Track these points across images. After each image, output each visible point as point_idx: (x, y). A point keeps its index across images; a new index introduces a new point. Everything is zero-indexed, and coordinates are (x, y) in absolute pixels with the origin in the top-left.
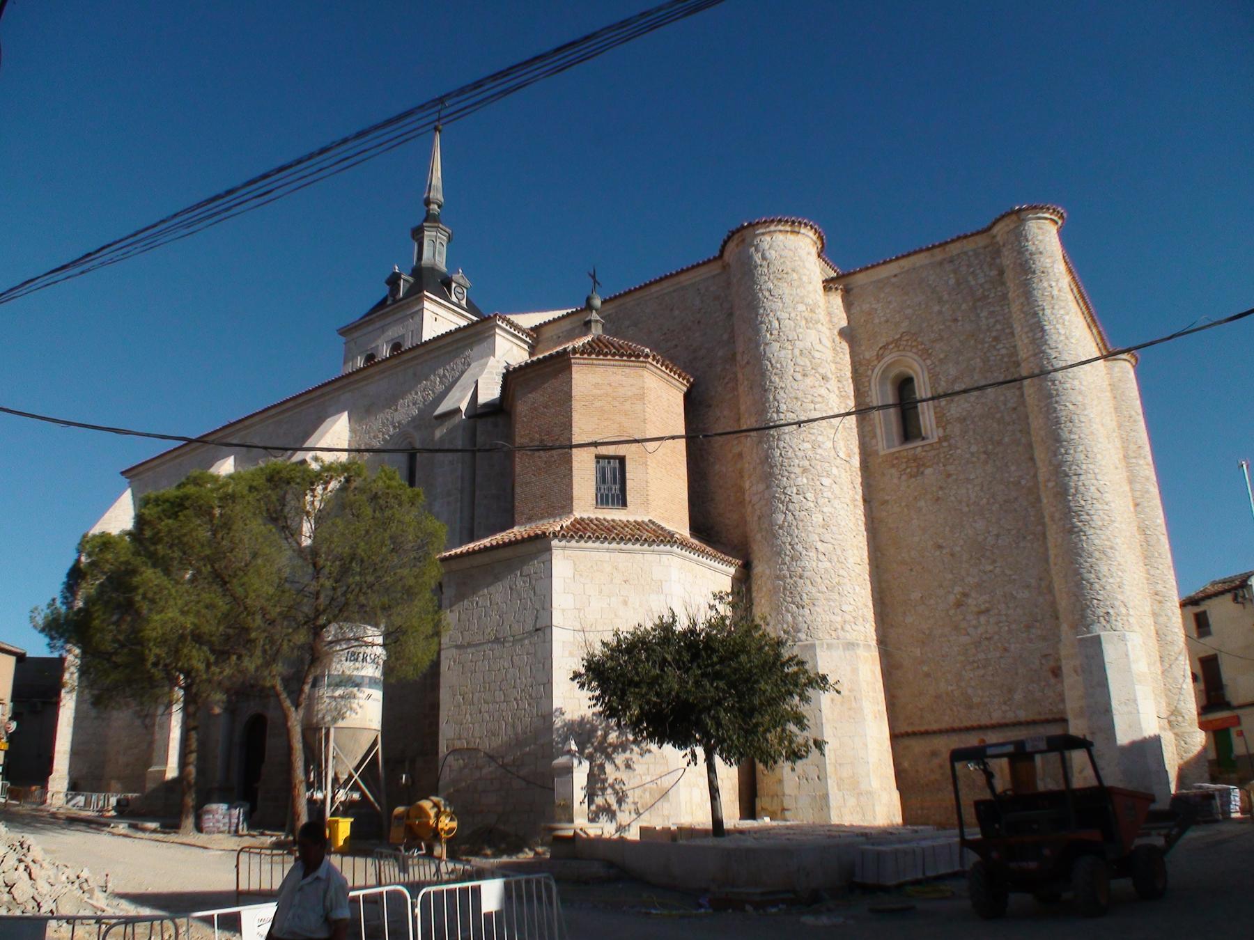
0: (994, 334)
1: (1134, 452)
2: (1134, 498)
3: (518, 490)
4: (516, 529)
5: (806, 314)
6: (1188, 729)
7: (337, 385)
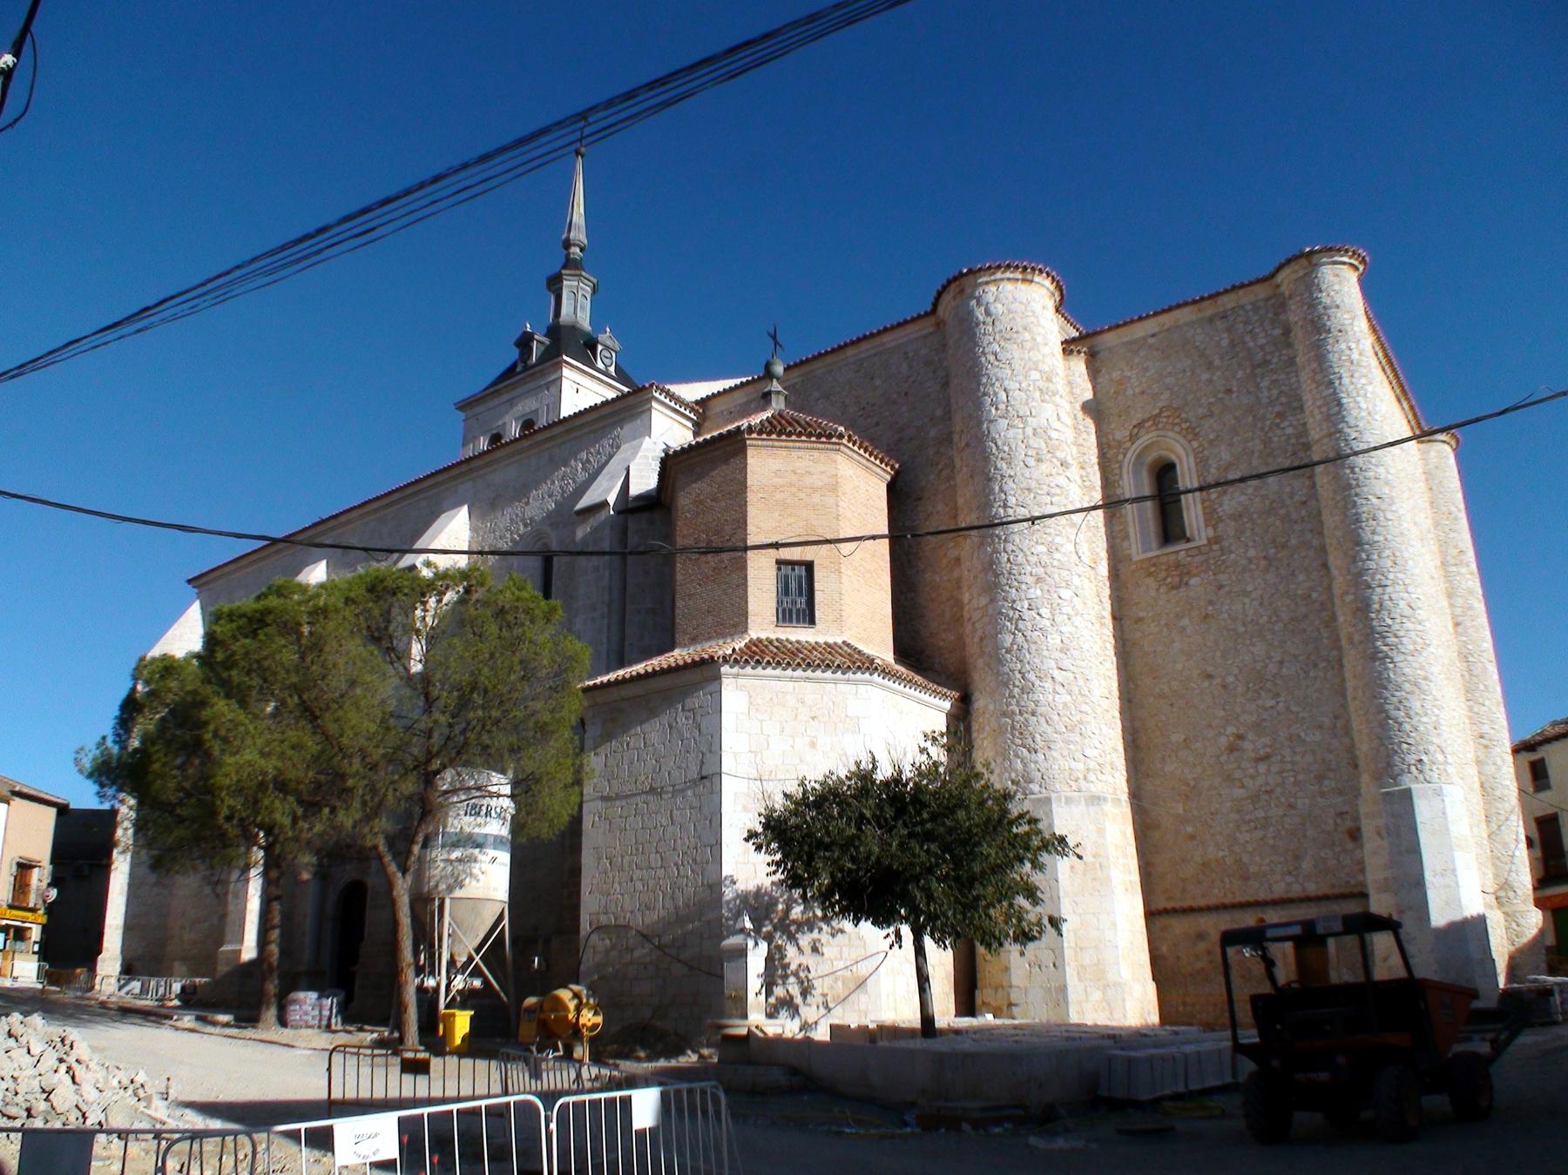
0: (1277, 409)
1: (1454, 557)
2: (1454, 616)
3: (680, 604)
4: (677, 652)
5: (1041, 384)
6: (1522, 907)
7: (455, 472)
